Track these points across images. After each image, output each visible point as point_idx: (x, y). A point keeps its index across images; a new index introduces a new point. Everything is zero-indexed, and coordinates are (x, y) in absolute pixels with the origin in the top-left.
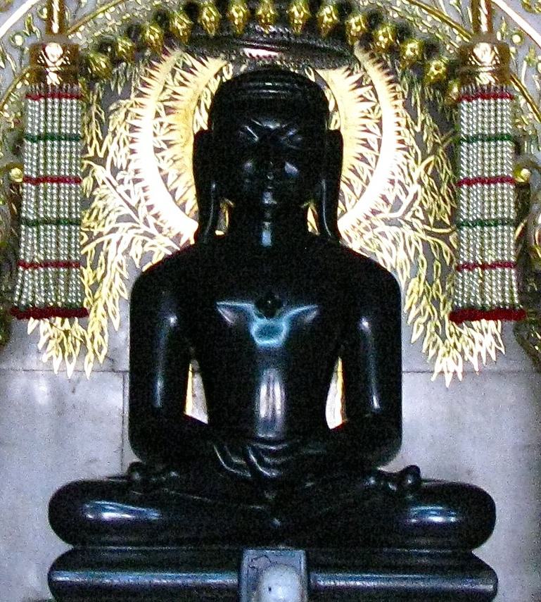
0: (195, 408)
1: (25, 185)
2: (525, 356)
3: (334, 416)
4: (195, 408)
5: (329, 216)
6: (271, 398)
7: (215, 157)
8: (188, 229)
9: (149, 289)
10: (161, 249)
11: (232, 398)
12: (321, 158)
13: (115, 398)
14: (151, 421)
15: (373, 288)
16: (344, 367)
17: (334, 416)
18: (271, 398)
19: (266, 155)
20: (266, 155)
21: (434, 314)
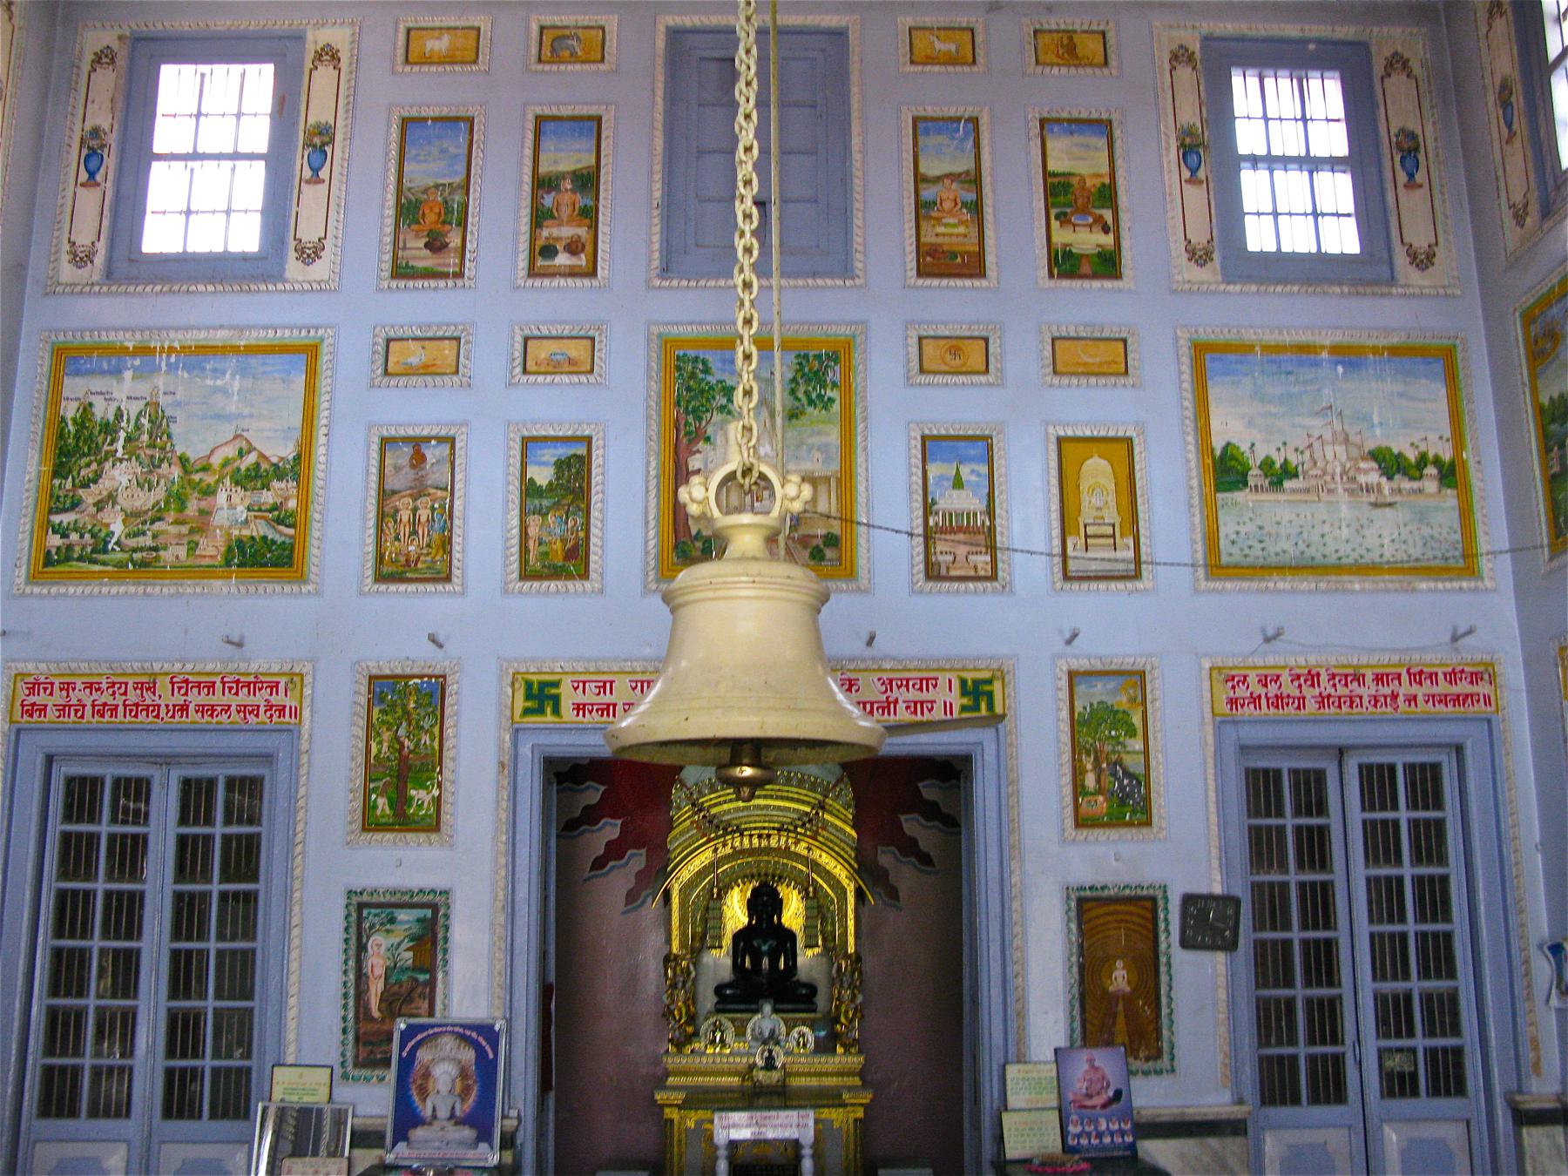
0: (747, 964)
1: (1129, 1139)
2: (389, 836)
3: (782, 966)
4: (747, 964)
5: (779, 919)
6: (765, 962)
7: (753, 906)
8: (746, 920)
9: (738, 937)
10: (741, 926)
11: (756, 962)
12: (777, 905)
13: (729, 962)
14: (737, 967)
15: (791, 935)
16: (557, 1100)
17: (782, 966)
18: (765, 962)
19: (765, 904)
20: (765, 904)
21: (1117, 912)
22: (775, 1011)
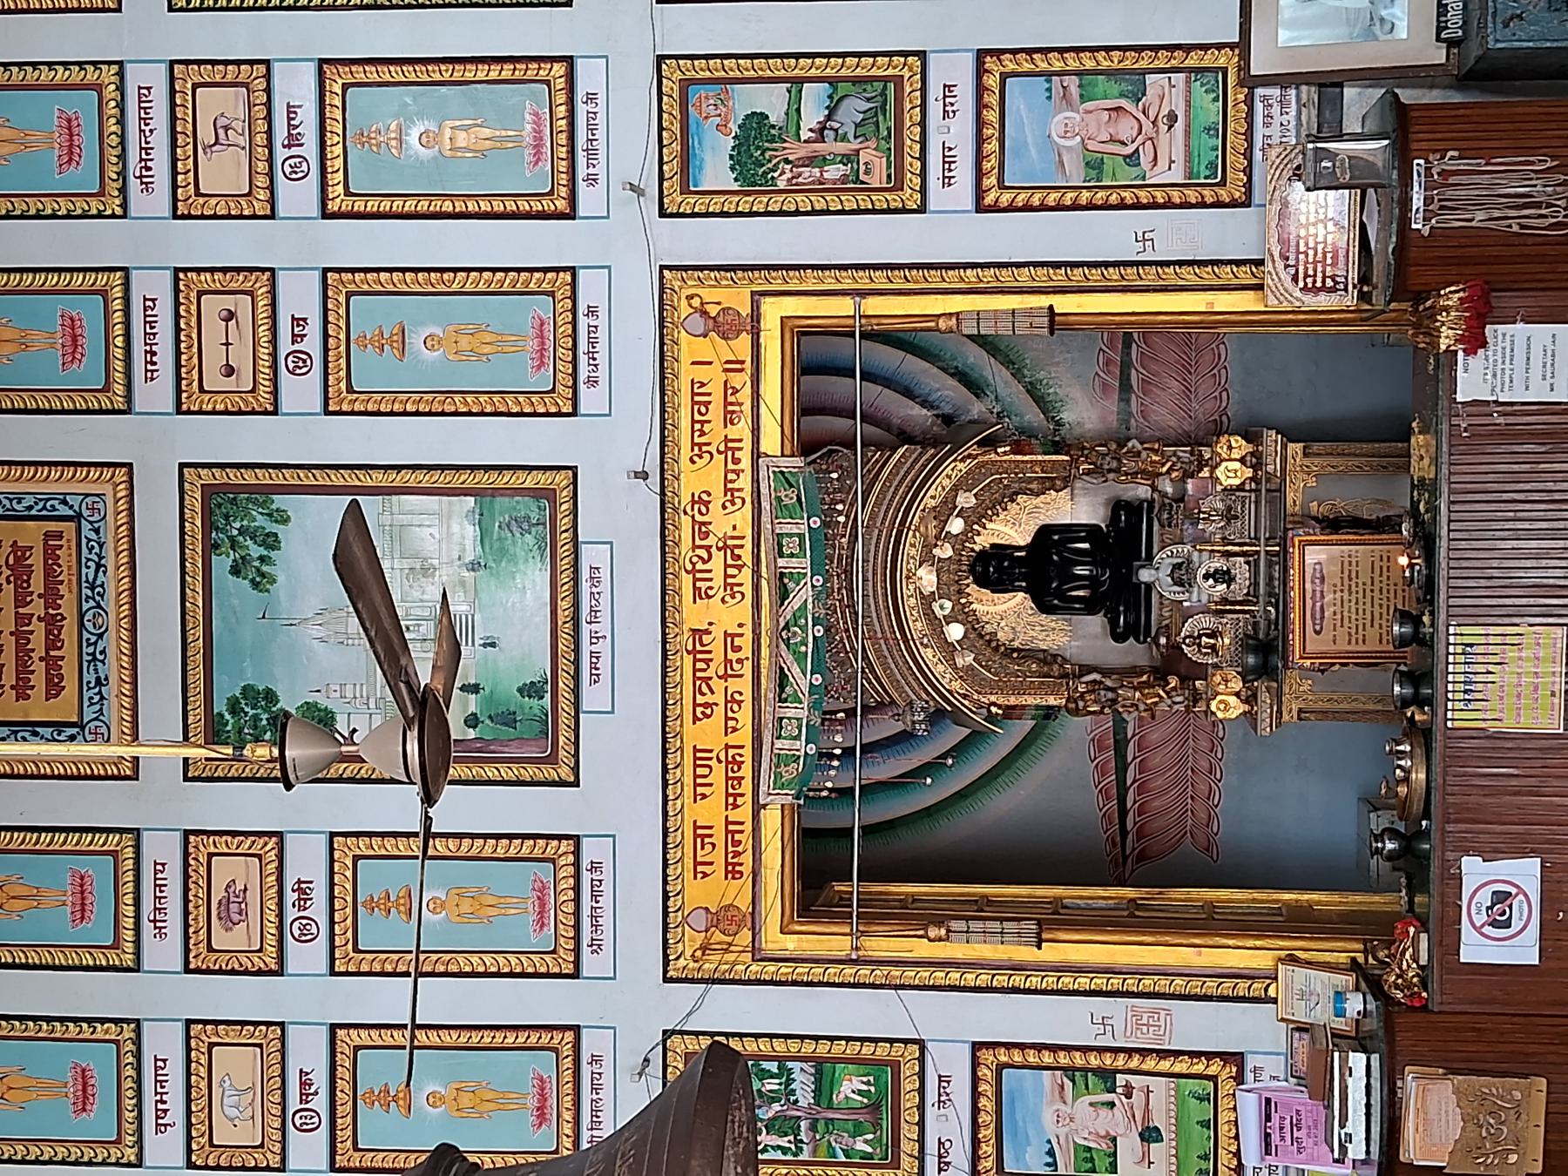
3: (1086, 546)
5: (1019, 548)
17: (1086, 546)
22: (1150, 557)
